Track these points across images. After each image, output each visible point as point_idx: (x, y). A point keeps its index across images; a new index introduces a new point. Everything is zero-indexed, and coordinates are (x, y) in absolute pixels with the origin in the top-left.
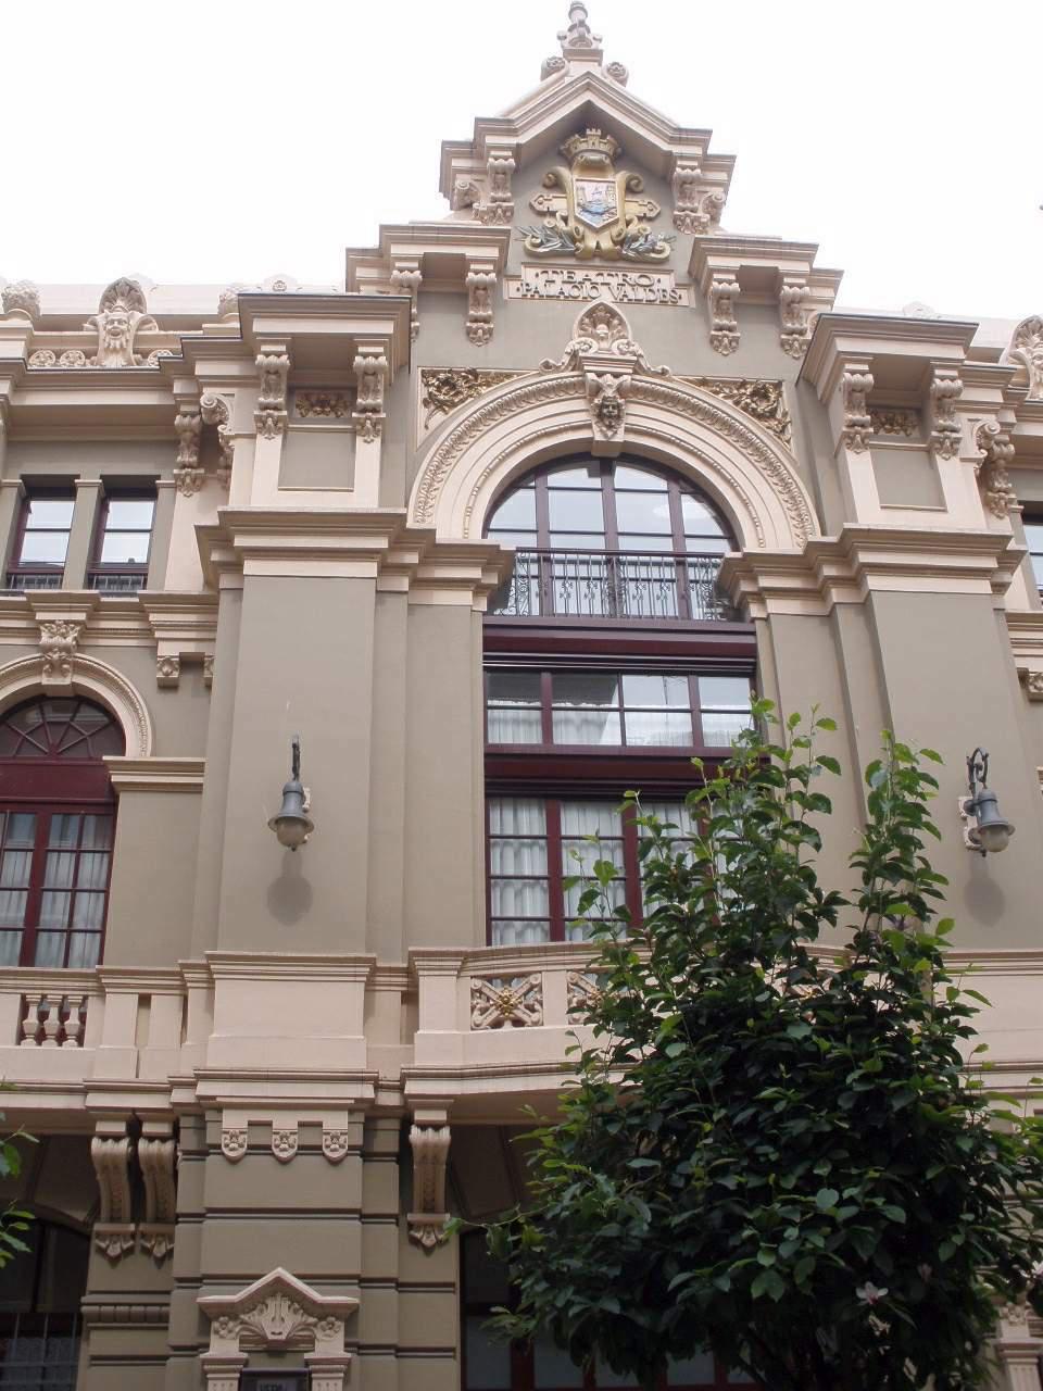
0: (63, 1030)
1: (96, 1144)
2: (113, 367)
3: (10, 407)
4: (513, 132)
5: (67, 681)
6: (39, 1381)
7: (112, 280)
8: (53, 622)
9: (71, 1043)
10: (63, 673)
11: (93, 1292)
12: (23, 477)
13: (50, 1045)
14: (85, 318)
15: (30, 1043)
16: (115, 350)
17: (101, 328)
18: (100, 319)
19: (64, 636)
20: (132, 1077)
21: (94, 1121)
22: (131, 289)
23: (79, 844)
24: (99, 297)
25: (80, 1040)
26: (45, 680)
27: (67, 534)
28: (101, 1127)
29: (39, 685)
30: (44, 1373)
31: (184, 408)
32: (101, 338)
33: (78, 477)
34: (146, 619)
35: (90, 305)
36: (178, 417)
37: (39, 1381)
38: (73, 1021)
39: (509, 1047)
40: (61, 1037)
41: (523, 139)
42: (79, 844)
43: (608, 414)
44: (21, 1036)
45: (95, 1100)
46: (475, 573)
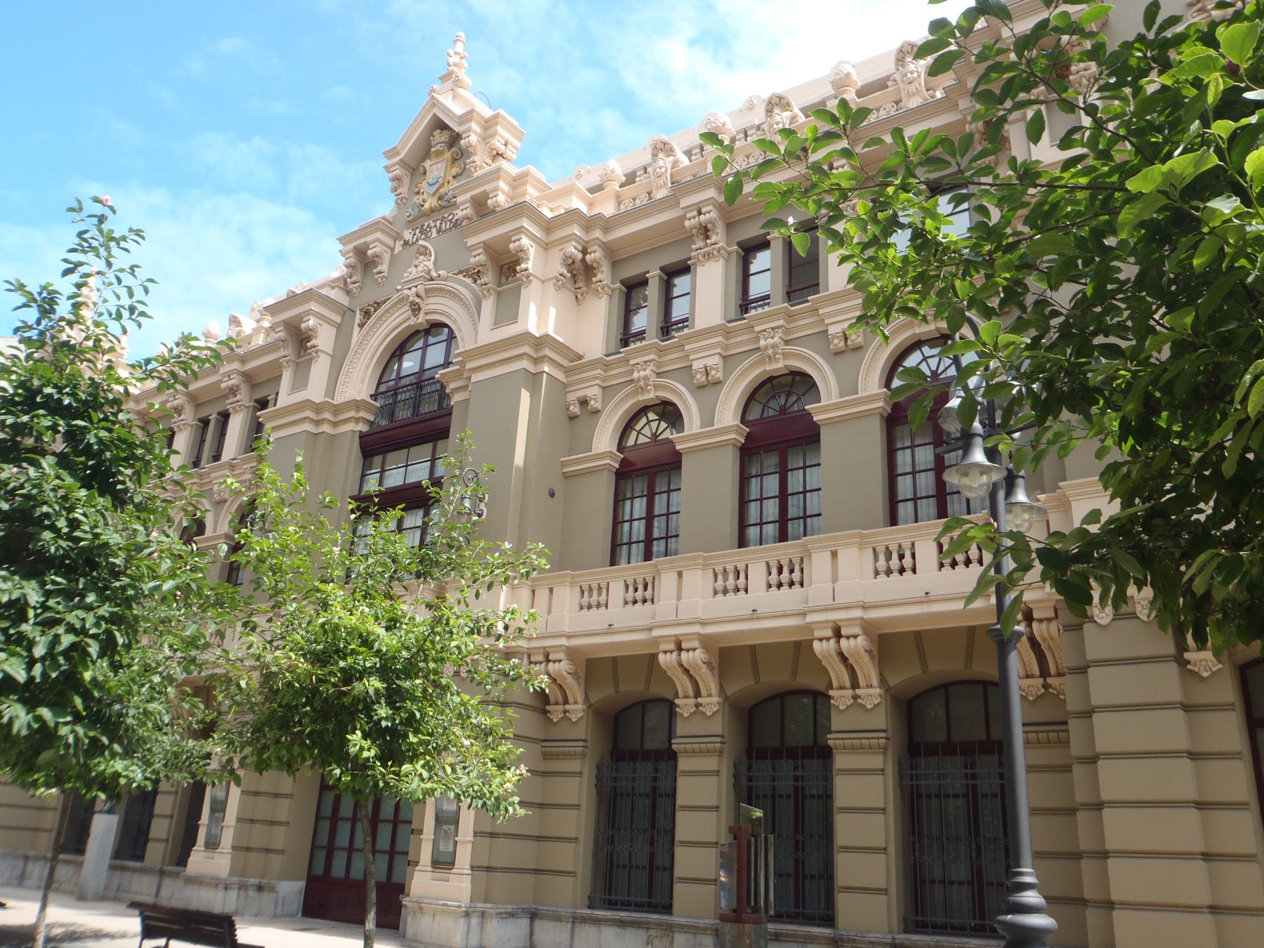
0: (968, 558)
1: (816, 645)
2: (915, 105)
3: (604, 243)
4: (398, 153)
5: (780, 365)
6: (909, 783)
7: (897, 45)
8: (765, 331)
9: (908, 574)
10: (777, 360)
11: (681, 737)
12: (739, 244)
13: (730, 596)
14: (888, 78)
15: (882, 577)
16: (913, 94)
17: (900, 82)
18: (897, 77)
19: (773, 338)
20: (674, 618)
21: (658, 644)
22: (780, 98)
23: (669, 487)
24: (893, 60)
25: (914, 570)
26: (918, 330)
27: (769, 272)
28: (818, 634)
29: (638, 401)
30: (774, 779)
31: (688, 215)
32: (902, 87)
33: (648, 272)
34: (818, 315)
35: (888, 67)
36: (967, 126)
37: (909, 783)
38: (907, 561)
39: (597, 619)
40: (902, 570)
41: (401, 156)
42: (669, 487)
43: (416, 309)
44: (877, 573)
45: (656, 633)
46: (352, 414)
